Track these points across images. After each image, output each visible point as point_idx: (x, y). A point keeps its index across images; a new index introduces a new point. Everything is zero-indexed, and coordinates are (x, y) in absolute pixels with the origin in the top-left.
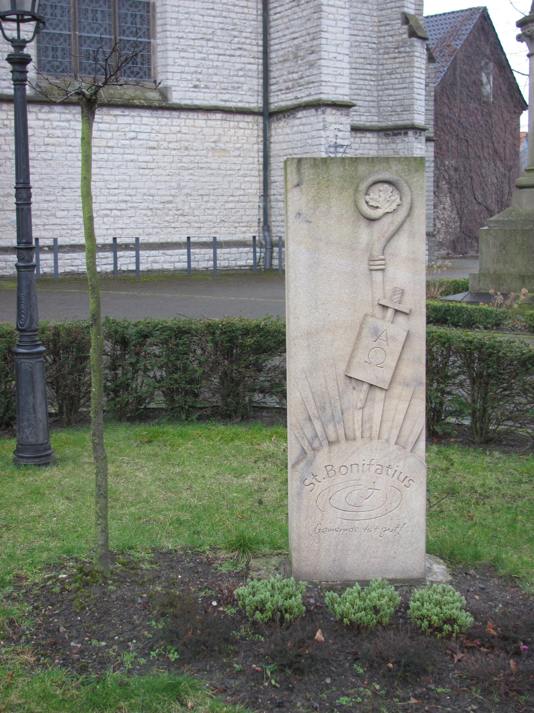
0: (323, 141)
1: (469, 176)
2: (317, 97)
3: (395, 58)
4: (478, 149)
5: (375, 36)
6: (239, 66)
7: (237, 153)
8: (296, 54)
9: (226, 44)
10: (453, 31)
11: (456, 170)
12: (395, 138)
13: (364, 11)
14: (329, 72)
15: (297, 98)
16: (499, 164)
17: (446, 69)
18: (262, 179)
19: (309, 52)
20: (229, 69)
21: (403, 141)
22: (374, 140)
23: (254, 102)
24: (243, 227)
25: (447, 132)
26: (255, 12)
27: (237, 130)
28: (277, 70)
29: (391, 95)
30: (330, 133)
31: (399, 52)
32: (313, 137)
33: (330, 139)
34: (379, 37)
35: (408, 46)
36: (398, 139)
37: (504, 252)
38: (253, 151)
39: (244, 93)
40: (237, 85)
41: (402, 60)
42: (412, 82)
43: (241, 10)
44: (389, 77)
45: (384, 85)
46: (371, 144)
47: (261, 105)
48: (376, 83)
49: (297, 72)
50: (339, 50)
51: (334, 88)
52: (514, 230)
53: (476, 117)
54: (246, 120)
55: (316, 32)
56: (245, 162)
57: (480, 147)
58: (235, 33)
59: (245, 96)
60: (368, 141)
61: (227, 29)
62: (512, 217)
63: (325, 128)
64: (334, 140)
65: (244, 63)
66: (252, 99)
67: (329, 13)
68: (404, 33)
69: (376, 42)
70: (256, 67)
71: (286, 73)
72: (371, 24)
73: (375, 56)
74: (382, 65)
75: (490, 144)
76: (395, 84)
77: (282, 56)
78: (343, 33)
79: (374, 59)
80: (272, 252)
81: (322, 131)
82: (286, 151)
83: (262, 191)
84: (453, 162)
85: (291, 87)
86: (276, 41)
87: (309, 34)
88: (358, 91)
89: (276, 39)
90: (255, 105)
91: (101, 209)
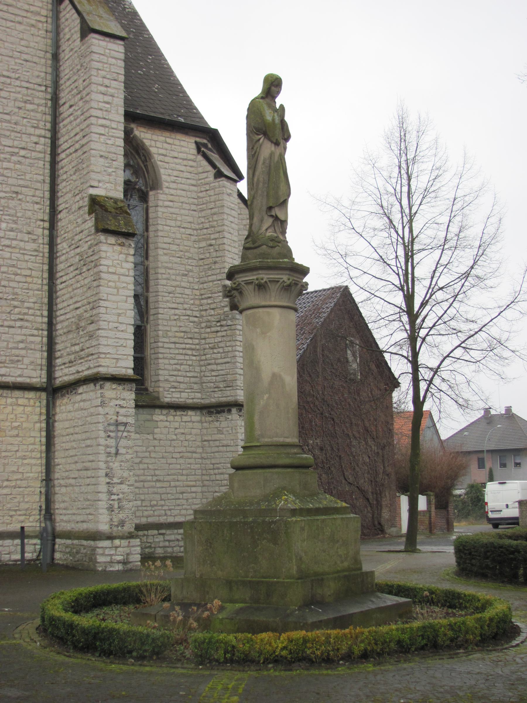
0: (101, 419)
1: (337, 456)
2: (95, 370)
3: (217, 332)
4: (346, 427)
5: (197, 309)
6: (19, 338)
7: (15, 432)
8: (78, 324)
9: (4, 315)
10: (315, 310)
11: (321, 449)
12: (219, 415)
13: (183, 284)
14: (109, 343)
15: (78, 372)
16: (370, 442)
17: (305, 346)
18: (44, 461)
19: (89, 322)
20: (8, 342)
21: (227, 419)
22: (198, 418)
23: (38, 377)
24: (20, 515)
25: (310, 410)
26: (40, 282)
27: (14, 407)
28: (62, 342)
29: (213, 371)
30: (110, 410)
31: (221, 326)
32: (92, 415)
33: (109, 417)
34: (201, 311)
35: (230, 319)
36: (222, 417)
37: (210, 551)
38: (34, 430)
39: (25, 367)
40: (16, 358)
41: (224, 333)
42: (235, 356)
43: (24, 279)
44: (211, 351)
45: (206, 360)
46: (194, 422)
47: (45, 380)
48: (198, 358)
49: (79, 344)
50: (121, 319)
51: (115, 361)
52: (221, 522)
53: (343, 395)
54: (26, 396)
55: (96, 301)
56: (24, 442)
57: (348, 425)
58: (16, 303)
59: (25, 371)
60: (189, 420)
61: (6, 299)
62: (221, 506)
63: (103, 404)
64: (115, 417)
65: (25, 335)
66: (34, 374)
67: (110, 281)
68: (226, 306)
69: (198, 315)
70: (40, 340)
71: (69, 345)
72: (192, 297)
73: (197, 330)
74: (205, 339)
75: (359, 422)
76: (217, 359)
77: (67, 327)
78: (126, 302)
79: (196, 333)
80: (54, 545)
81: (100, 408)
82: (68, 430)
83: (44, 474)
84: (318, 441)
85: (73, 360)
86: (62, 312)
87: (89, 303)
88: (178, 367)
89: (62, 309)
90: (38, 380)
91: (166, 487)
